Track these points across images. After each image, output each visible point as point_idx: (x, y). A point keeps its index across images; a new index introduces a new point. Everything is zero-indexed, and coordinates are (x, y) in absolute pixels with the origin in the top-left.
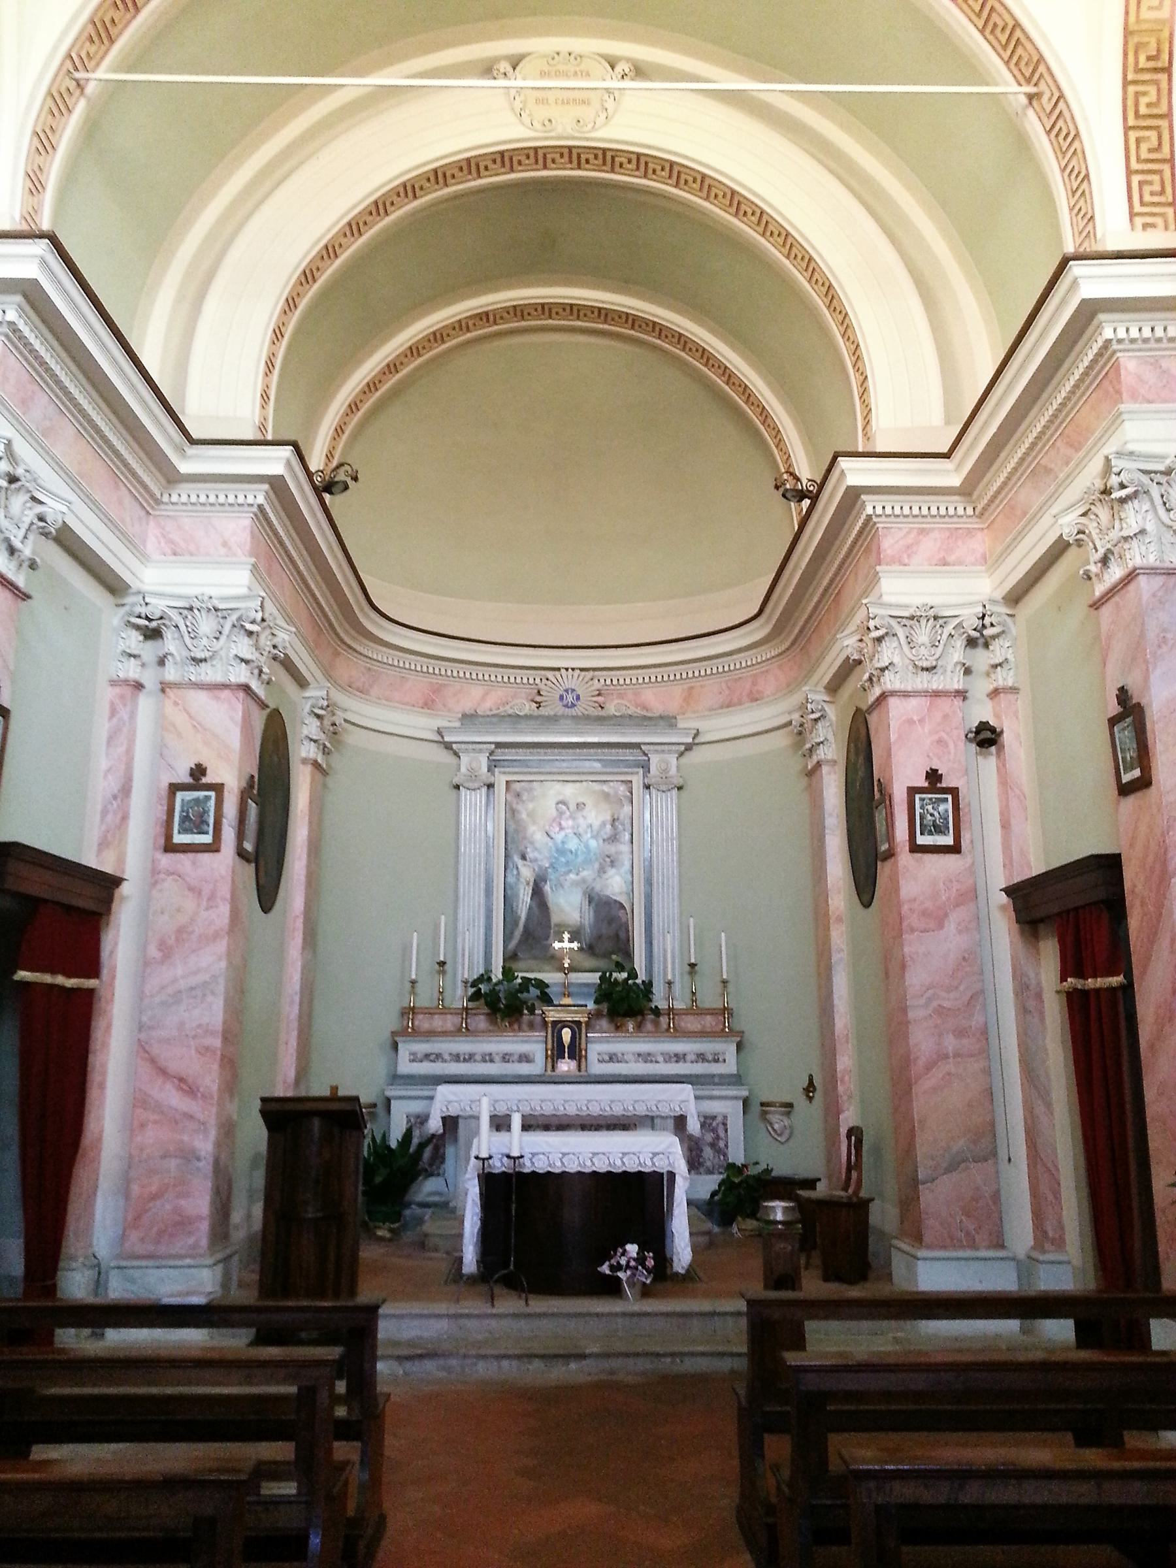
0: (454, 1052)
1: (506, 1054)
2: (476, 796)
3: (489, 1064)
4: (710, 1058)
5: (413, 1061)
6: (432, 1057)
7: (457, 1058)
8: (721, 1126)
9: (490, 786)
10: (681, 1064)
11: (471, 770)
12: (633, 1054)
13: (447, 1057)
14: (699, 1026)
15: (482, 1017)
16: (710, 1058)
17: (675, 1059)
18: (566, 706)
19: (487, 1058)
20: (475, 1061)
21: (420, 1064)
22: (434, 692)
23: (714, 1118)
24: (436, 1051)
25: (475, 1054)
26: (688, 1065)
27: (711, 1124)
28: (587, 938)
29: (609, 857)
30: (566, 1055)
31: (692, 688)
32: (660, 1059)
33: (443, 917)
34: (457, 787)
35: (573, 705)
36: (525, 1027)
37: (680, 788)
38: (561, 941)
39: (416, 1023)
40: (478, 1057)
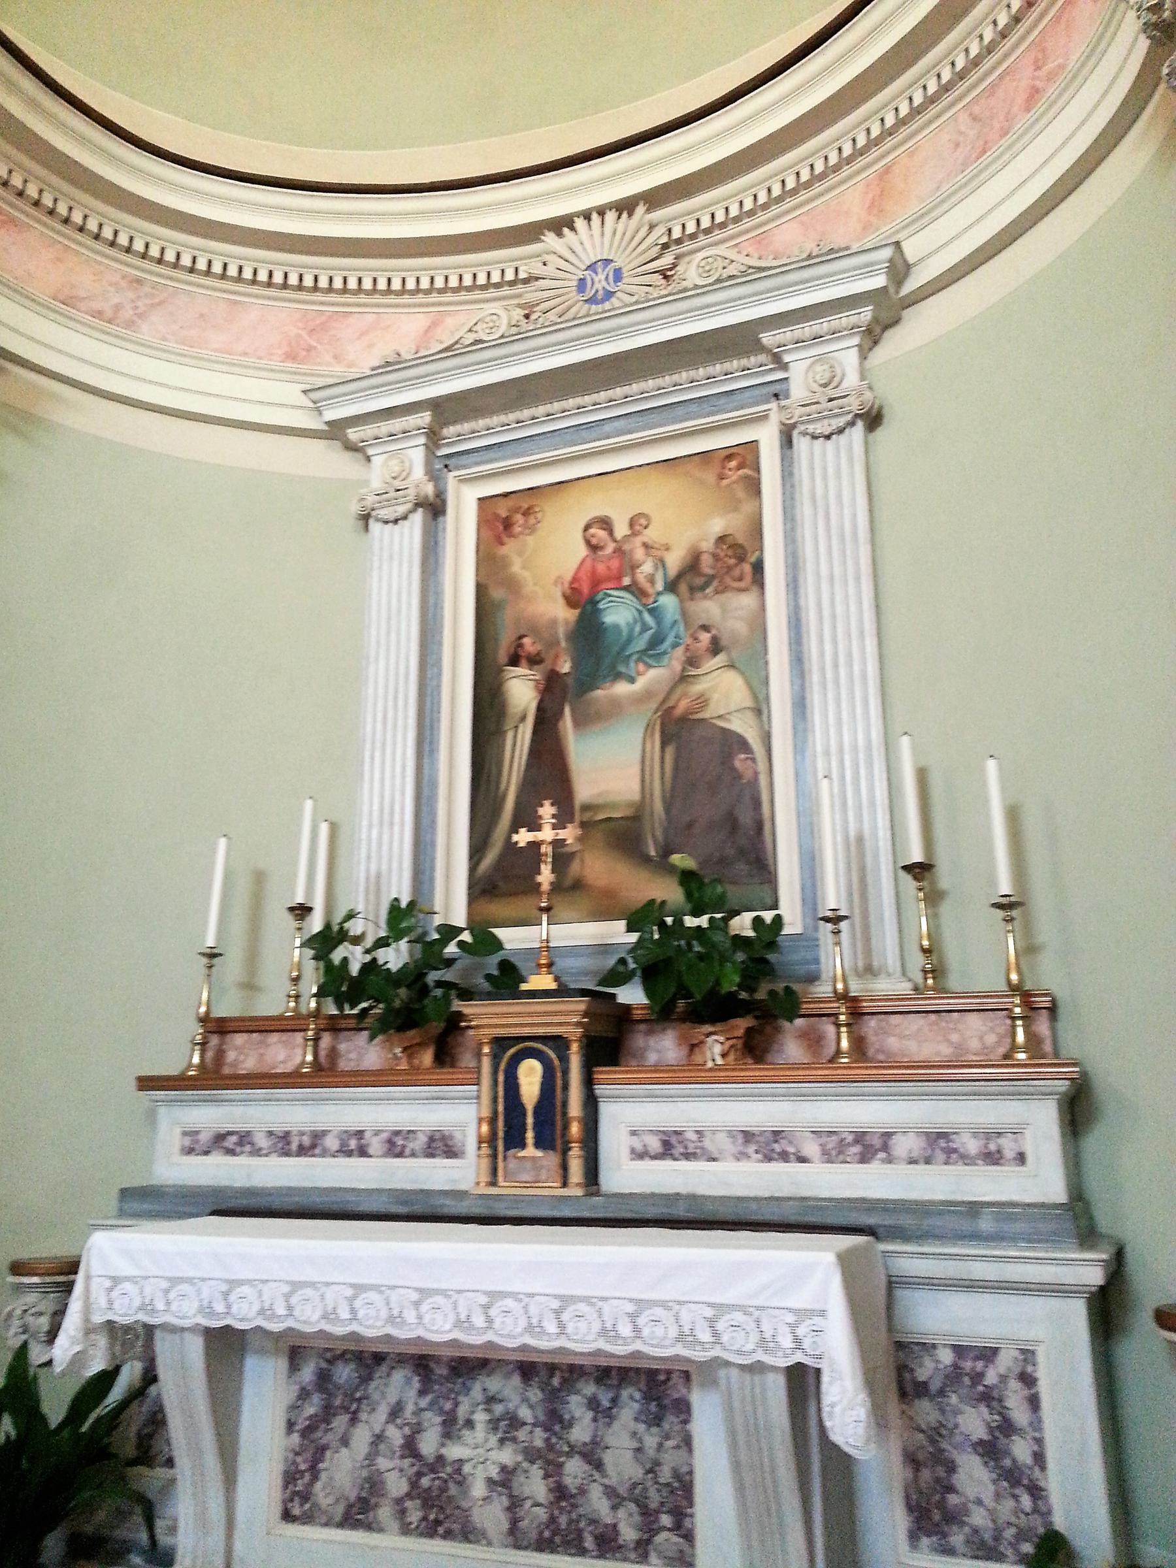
0: (278, 1129)
1: (397, 1133)
2: (402, 534)
3: (356, 1162)
4: (972, 1146)
5: (190, 1151)
7: (284, 1144)
8: (1014, 1385)
9: (435, 508)
12: (731, 1134)
13: (262, 1142)
16: (972, 1146)
17: (856, 1149)
20: (325, 1153)
23: (989, 1354)
25: (324, 1133)
26: (902, 1169)
27: (977, 1377)
28: (659, 833)
29: (705, 628)
30: (530, 1135)
32: (811, 1148)
35: (609, 295)
37: (873, 419)
38: (535, 826)
40: (332, 1143)
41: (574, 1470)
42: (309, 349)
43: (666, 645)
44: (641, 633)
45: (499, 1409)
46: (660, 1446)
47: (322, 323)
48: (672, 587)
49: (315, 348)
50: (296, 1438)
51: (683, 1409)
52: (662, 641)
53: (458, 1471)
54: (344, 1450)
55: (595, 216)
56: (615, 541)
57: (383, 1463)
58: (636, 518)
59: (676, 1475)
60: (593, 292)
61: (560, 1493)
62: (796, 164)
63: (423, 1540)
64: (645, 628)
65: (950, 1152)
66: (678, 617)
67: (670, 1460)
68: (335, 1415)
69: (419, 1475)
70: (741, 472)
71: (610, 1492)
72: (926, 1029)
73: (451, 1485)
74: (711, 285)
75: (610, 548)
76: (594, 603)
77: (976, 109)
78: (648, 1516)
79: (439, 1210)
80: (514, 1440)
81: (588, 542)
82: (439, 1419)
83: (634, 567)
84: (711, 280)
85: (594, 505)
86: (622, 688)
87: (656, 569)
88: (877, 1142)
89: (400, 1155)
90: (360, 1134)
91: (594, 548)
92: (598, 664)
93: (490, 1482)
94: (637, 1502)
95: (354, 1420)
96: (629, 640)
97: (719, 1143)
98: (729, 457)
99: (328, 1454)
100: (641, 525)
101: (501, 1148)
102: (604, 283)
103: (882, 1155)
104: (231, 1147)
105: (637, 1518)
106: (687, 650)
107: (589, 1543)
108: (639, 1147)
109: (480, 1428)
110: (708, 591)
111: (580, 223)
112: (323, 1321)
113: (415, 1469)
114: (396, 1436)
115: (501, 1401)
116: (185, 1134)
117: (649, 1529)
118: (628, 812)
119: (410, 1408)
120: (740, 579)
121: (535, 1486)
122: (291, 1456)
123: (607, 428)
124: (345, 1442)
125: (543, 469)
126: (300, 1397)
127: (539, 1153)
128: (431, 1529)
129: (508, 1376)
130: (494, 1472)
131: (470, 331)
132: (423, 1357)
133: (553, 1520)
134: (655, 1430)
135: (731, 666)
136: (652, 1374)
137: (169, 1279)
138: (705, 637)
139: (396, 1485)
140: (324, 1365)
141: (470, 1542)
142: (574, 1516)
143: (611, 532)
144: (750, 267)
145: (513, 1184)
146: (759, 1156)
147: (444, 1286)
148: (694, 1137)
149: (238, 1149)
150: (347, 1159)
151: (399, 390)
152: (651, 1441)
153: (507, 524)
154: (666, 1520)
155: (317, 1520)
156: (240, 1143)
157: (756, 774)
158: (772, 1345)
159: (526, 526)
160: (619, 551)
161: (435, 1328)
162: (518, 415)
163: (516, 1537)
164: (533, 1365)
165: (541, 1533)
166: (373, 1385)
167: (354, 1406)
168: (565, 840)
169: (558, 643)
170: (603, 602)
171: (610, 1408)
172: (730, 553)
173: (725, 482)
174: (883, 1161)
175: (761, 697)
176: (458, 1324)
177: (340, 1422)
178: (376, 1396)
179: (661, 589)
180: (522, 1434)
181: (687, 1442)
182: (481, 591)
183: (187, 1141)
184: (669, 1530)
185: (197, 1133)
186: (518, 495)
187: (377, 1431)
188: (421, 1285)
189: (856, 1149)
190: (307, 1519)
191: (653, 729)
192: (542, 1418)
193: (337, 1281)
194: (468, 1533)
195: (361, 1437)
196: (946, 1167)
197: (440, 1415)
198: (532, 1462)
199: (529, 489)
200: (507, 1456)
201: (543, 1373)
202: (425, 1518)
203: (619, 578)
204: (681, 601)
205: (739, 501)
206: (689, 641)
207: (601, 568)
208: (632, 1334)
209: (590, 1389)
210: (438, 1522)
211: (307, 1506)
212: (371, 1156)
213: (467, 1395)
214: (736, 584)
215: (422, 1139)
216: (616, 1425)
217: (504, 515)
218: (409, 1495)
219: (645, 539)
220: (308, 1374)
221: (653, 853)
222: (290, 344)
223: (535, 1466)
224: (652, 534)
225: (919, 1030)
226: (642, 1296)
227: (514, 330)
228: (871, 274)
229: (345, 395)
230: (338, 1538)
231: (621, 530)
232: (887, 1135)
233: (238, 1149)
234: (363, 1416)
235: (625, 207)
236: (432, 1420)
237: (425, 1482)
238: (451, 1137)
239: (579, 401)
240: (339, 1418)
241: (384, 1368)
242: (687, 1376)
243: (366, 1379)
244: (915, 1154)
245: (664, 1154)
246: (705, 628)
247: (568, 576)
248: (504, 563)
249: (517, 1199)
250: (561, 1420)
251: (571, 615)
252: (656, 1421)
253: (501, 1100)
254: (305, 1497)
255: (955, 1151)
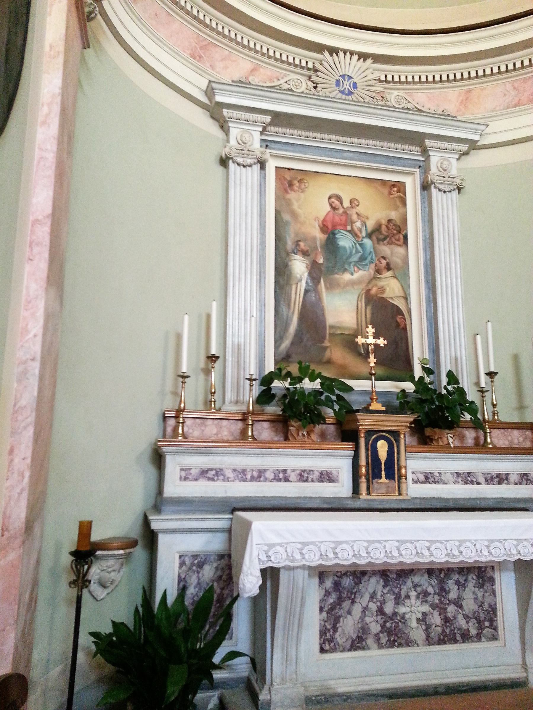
0: (240, 468)
1: (304, 471)
3: (283, 484)
5: (186, 479)
6: (211, 474)
10: (504, 486)
11: (242, 142)
13: (229, 474)
14: (507, 443)
15: (266, 425)
17: (497, 479)
18: (342, 92)
19: (281, 476)
20: (266, 480)
21: (195, 483)
22: (201, 47)
24: (217, 467)
25: (265, 470)
29: (384, 258)
30: (383, 473)
31: (470, 91)
32: (482, 479)
33: (186, 317)
34: (224, 162)
36: (314, 437)
39: (186, 429)
40: (269, 475)
41: (451, 609)
42: (200, 57)
43: (367, 262)
44: (355, 254)
45: (419, 589)
46: (484, 596)
47: (206, 45)
48: (369, 236)
49: (202, 57)
50: (324, 614)
51: (492, 580)
52: (365, 259)
53: (403, 618)
54: (349, 616)
55: (348, 54)
56: (343, 208)
57: (368, 620)
58: (353, 200)
59: (490, 606)
60: (343, 88)
61: (446, 620)
62: (442, 71)
63: (390, 650)
64: (357, 252)
65: (527, 480)
66: (372, 250)
67: (488, 600)
68: (344, 601)
69: (385, 622)
70: (399, 194)
71: (466, 617)
72: (500, 435)
73: (400, 624)
74: (399, 108)
75: (341, 211)
76: (334, 234)
77: (516, 85)
78: (480, 622)
79: (297, 505)
80: (426, 601)
81: (331, 205)
82: (393, 597)
83: (352, 223)
84: (401, 107)
85: (334, 188)
86: (347, 276)
87: (362, 225)
88: (504, 477)
89: (306, 481)
90: (285, 471)
91: (334, 208)
92: (336, 263)
93: (418, 620)
94: (476, 619)
95: (353, 602)
96: (351, 255)
97: (448, 477)
98: (394, 186)
99: (341, 619)
100: (355, 204)
101: (370, 478)
102: (348, 86)
103: (506, 482)
104: (212, 477)
105: (477, 625)
106: (376, 265)
107: (458, 638)
108: (416, 479)
109: (413, 598)
110: (385, 242)
111: (341, 54)
112: (505, 556)
113: (383, 620)
114: (373, 607)
115: (420, 586)
116: (182, 470)
117: (481, 628)
118: (351, 332)
119: (379, 594)
120: (398, 240)
121: (436, 619)
122: (323, 623)
123: (345, 154)
124: (349, 613)
125: (296, 161)
126: (325, 595)
127: (387, 481)
128: (392, 644)
129: (422, 575)
130: (420, 616)
131: (286, 82)
132: (384, 571)
133: (444, 631)
134: (481, 590)
135: (395, 277)
136: (480, 568)
137: (368, 541)
138: (384, 262)
139: (375, 628)
140: (336, 578)
141: (410, 646)
142: (452, 628)
143: (341, 203)
144: (416, 108)
145: (377, 494)
146: (463, 482)
147: (439, 539)
148: (438, 475)
149: (216, 478)
150: (279, 483)
151: (261, 101)
152: (480, 594)
153: (291, 184)
154: (487, 624)
155: (338, 650)
156: (217, 474)
157: (406, 325)
158: (509, 553)
159: (300, 187)
160: (345, 213)
161: (438, 557)
162: (307, 134)
163: (429, 641)
164: (432, 569)
165: (439, 638)
166: (361, 585)
167: (353, 596)
168: (380, 344)
169: (317, 249)
170: (338, 235)
171: (464, 584)
172: (394, 227)
173: (392, 196)
174: (506, 484)
175: (407, 293)
176: (321, 557)
177: (346, 604)
178: (363, 590)
179: (364, 236)
180: (429, 598)
181: (494, 593)
182: (278, 213)
183: (183, 474)
184: (488, 627)
185: (190, 469)
186: (304, 172)
187: (364, 606)
188: (430, 539)
189: (497, 479)
190: (333, 650)
191: (362, 298)
192: (437, 591)
193: (391, 539)
194: (409, 643)
195: (357, 610)
196: (527, 486)
197: (394, 595)
198: (434, 609)
199: (301, 170)
200: (426, 608)
201: (437, 573)
202: (389, 640)
203: (345, 226)
204: (374, 244)
205: (398, 207)
206: (377, 262)
207: (337, 219)
208: (334, 556)
209: (456, 577)
210: (395, 641)
211: (332, 644)
212: (291, 482)
213: (405, 585)
214: (397, 242)
215: (317, 474)
216: (467, 589)
217: (289, 179)
218: (381, 632)
219: (358, 211)
220: (329, 584)
221: (363, 352)
222: (192, 49)
223: (435, 611)
224: (360, 209)
225: (498, 435)
226: (519, 538)
227: (307, 91)
228: (475, 133)
229: (256, 95)
230: (350, 656)
231: (346, 204)
232: (507, 475)
233: (216, 478)
234: (358, 600)
235: (364, 56)
236: (390, 598)
237: (388, 625)
238: (331, 473)
239: (338, 138)
240: (346, 602)
241: (366, 578)
242: (493, 567)
243: (357, 584)
244: (516, 481)
245: (426, 481)
246: (384, 258)
247: (322, 218)
248: (289, 203)
249: (381, 501)
250: (445, 590)
251: (323, 237)
252: (481, 586)
253: (370, 458)
254: (331, 641)
255: (529, 480)
